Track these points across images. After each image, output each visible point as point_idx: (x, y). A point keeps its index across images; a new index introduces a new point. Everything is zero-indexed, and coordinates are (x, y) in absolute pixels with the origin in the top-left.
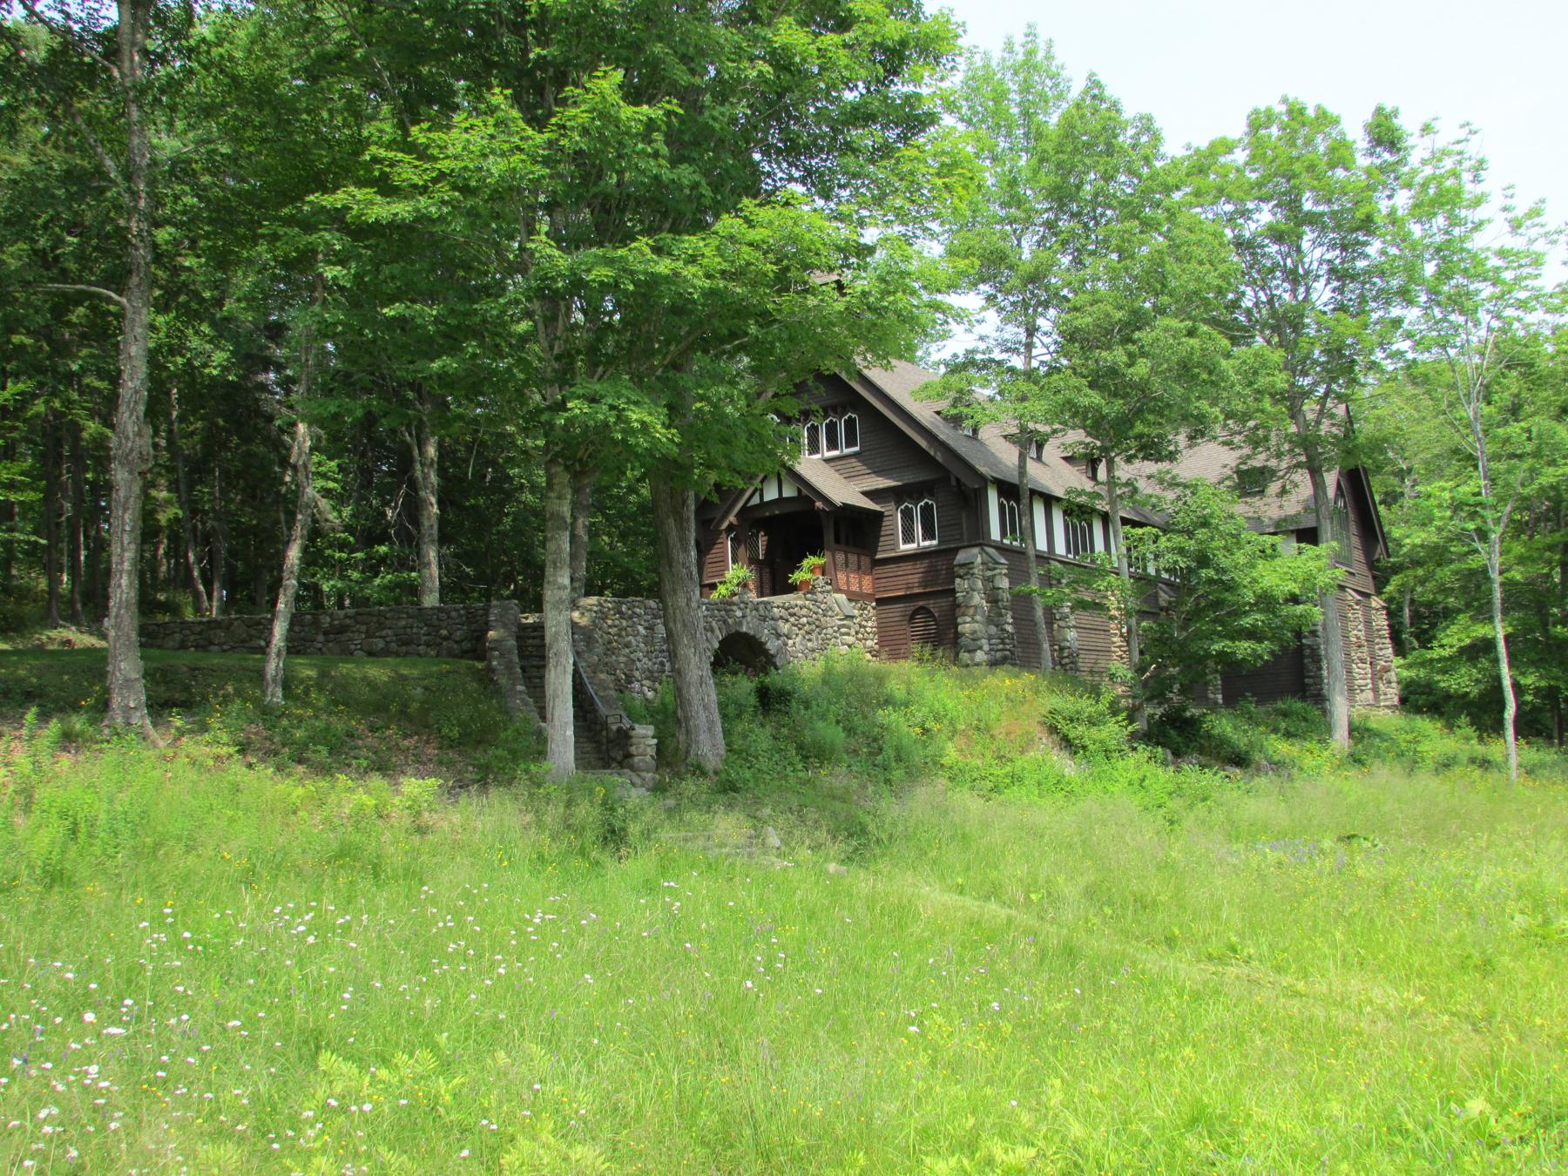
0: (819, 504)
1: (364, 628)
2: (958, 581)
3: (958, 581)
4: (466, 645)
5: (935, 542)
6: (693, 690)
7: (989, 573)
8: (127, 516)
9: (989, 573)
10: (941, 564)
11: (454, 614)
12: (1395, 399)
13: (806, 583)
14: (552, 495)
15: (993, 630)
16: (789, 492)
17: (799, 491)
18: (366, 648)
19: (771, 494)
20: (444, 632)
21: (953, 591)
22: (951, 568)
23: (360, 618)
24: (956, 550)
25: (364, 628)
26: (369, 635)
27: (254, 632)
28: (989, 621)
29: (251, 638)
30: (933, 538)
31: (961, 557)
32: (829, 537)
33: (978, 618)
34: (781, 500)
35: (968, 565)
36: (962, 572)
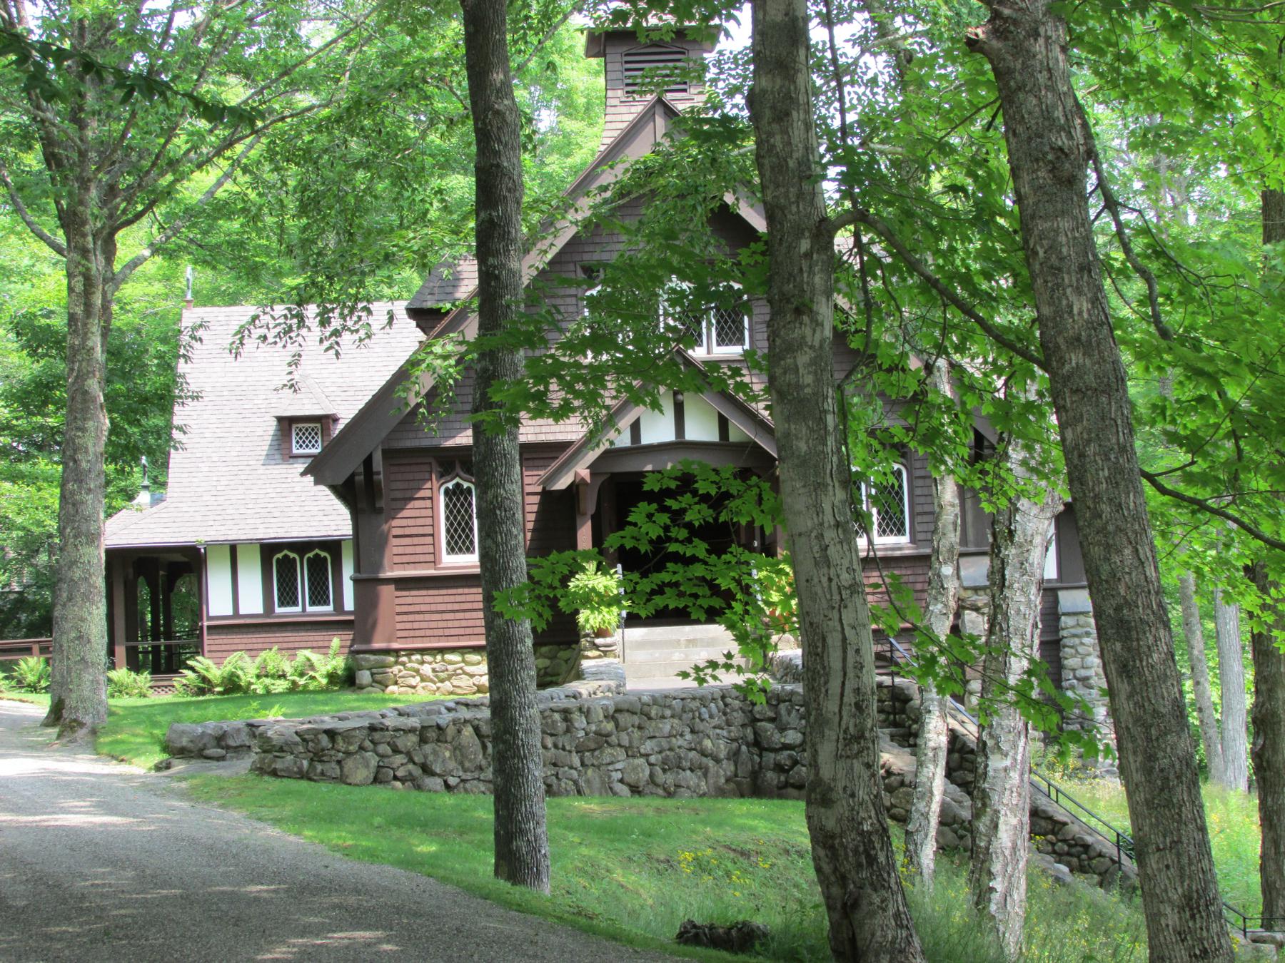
5: (904, 540)
17: (723, 424)
30: (900, 531)
34: (681, 445)
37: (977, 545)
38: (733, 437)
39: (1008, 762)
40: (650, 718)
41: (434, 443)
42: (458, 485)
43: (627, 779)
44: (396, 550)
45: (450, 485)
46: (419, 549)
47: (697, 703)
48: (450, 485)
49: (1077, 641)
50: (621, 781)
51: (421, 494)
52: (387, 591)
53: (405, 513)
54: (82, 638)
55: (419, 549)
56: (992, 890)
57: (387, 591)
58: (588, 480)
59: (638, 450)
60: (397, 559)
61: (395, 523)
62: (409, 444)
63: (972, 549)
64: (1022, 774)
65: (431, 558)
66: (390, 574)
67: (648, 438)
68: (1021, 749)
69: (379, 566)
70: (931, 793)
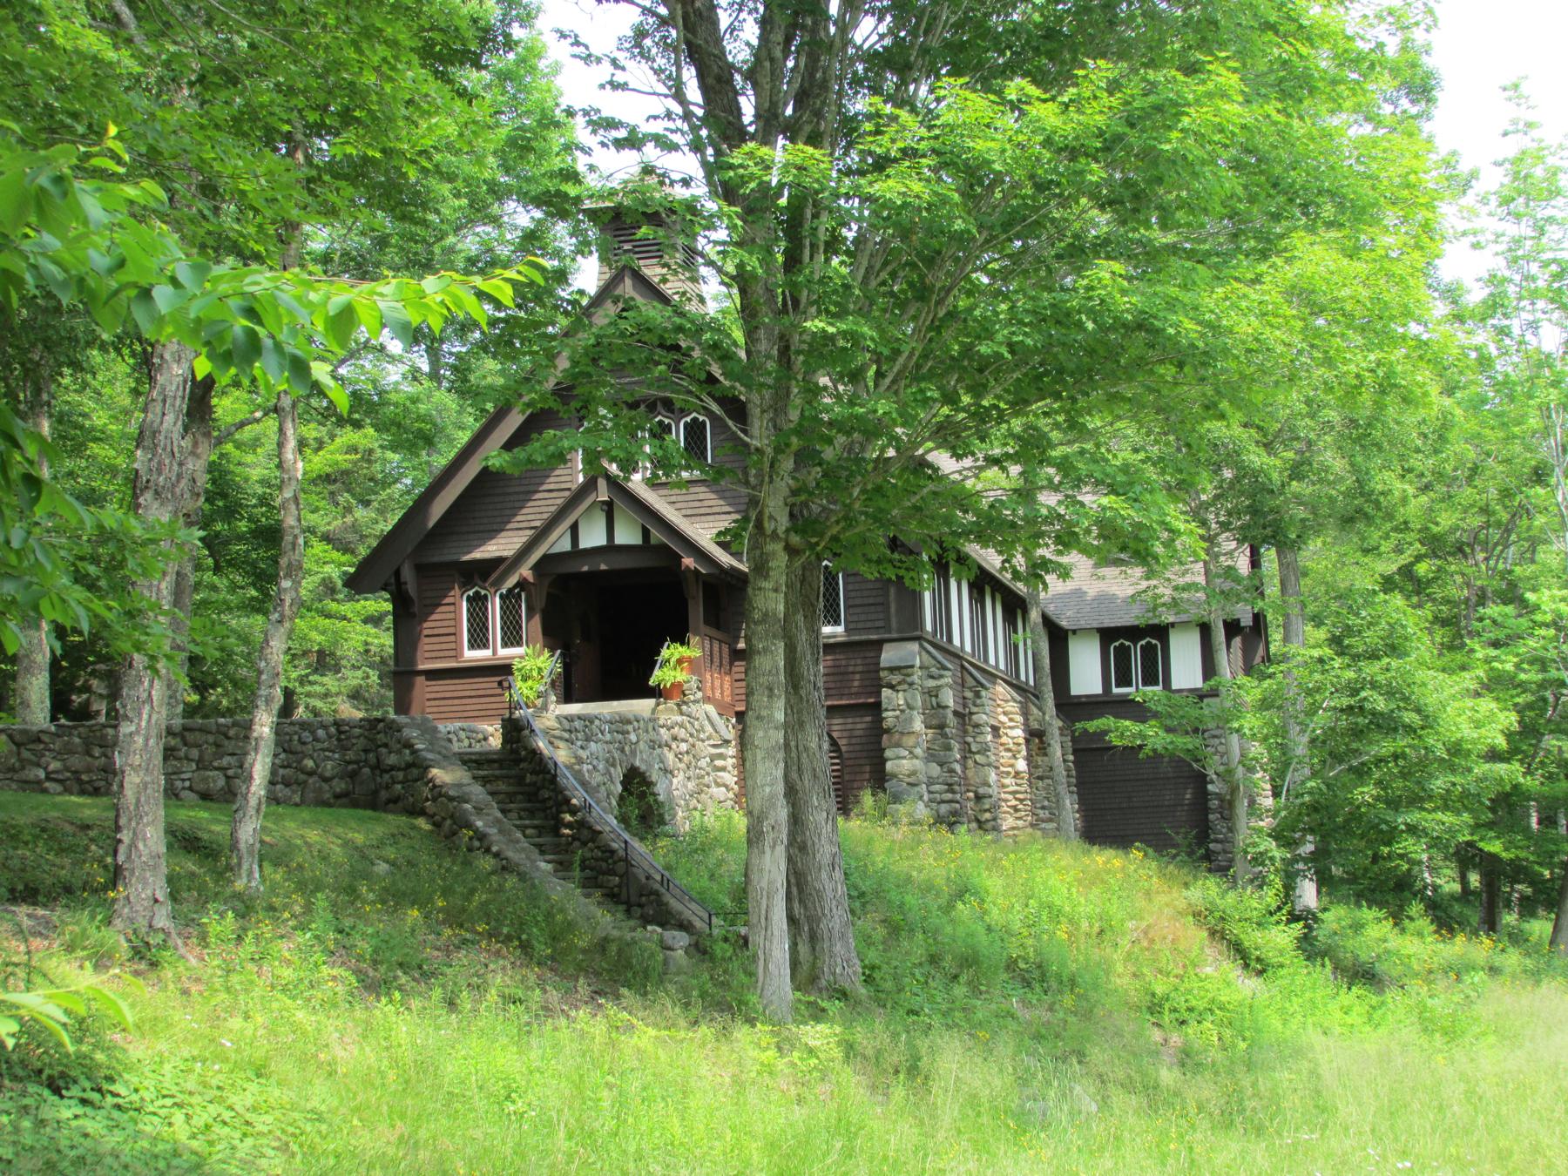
0: (688, 562)
1: (195, 753)
2: (886, 692)
3: (886, 692)
4: (340, 786)
5: (840, 629)
6: (824, 875)
7: (931, 683)
8: (164, 585)
9: (931, 683)
10: (856, 663)
11: (321, 733)
12: (90, 200)
13: (678, 687)
14: (767, 585)
15: (935, 770)
16: (626, 535)
17: (646, 533)
18: (201, 787)
19: (593, 537)
20: (309, 763)
21: (877, 708)
22: (876, 668)
23: (190, 737)
24: (878, 645)
25: (195, 753)
26: (202, 765)
27: (26, 754)
28: (931, 756)
29: (24, 764)
30: (837, 622)
31: (890, 655)
32: (696, 612)
33: (918, 751)
34: (611, 549)
35: (902, 669)
36: (895, 678)
37: (899, 631)
38: (653, 541)
39: (133, 728)
40: (228, 738)
41: (455, 558)
42: (477, 593)
43: (196, 788)
44: (427, 648)
45: (471, 593)
46: (444, 646)
47: (297, 728)
48: (471, 593)
49: (1217, 741)
50: (191, 789)
51: (447, 600)
52: (421, 686)
53: (434, 617)
54: (25, 704)
55: (444, 646)
56: (120, 841)
57: (420, 680)
58: (531, 580)
59: (577, 553)
60: (427, 655)
61: (425, 625)
62: (436, 559)
63: (895, 635)
64: (147, 740)
65: (452, 653)
66: (421, 667)
67: (585, 543)
68: (145, 716)
69: (413, 662)
70: (251, 777)
